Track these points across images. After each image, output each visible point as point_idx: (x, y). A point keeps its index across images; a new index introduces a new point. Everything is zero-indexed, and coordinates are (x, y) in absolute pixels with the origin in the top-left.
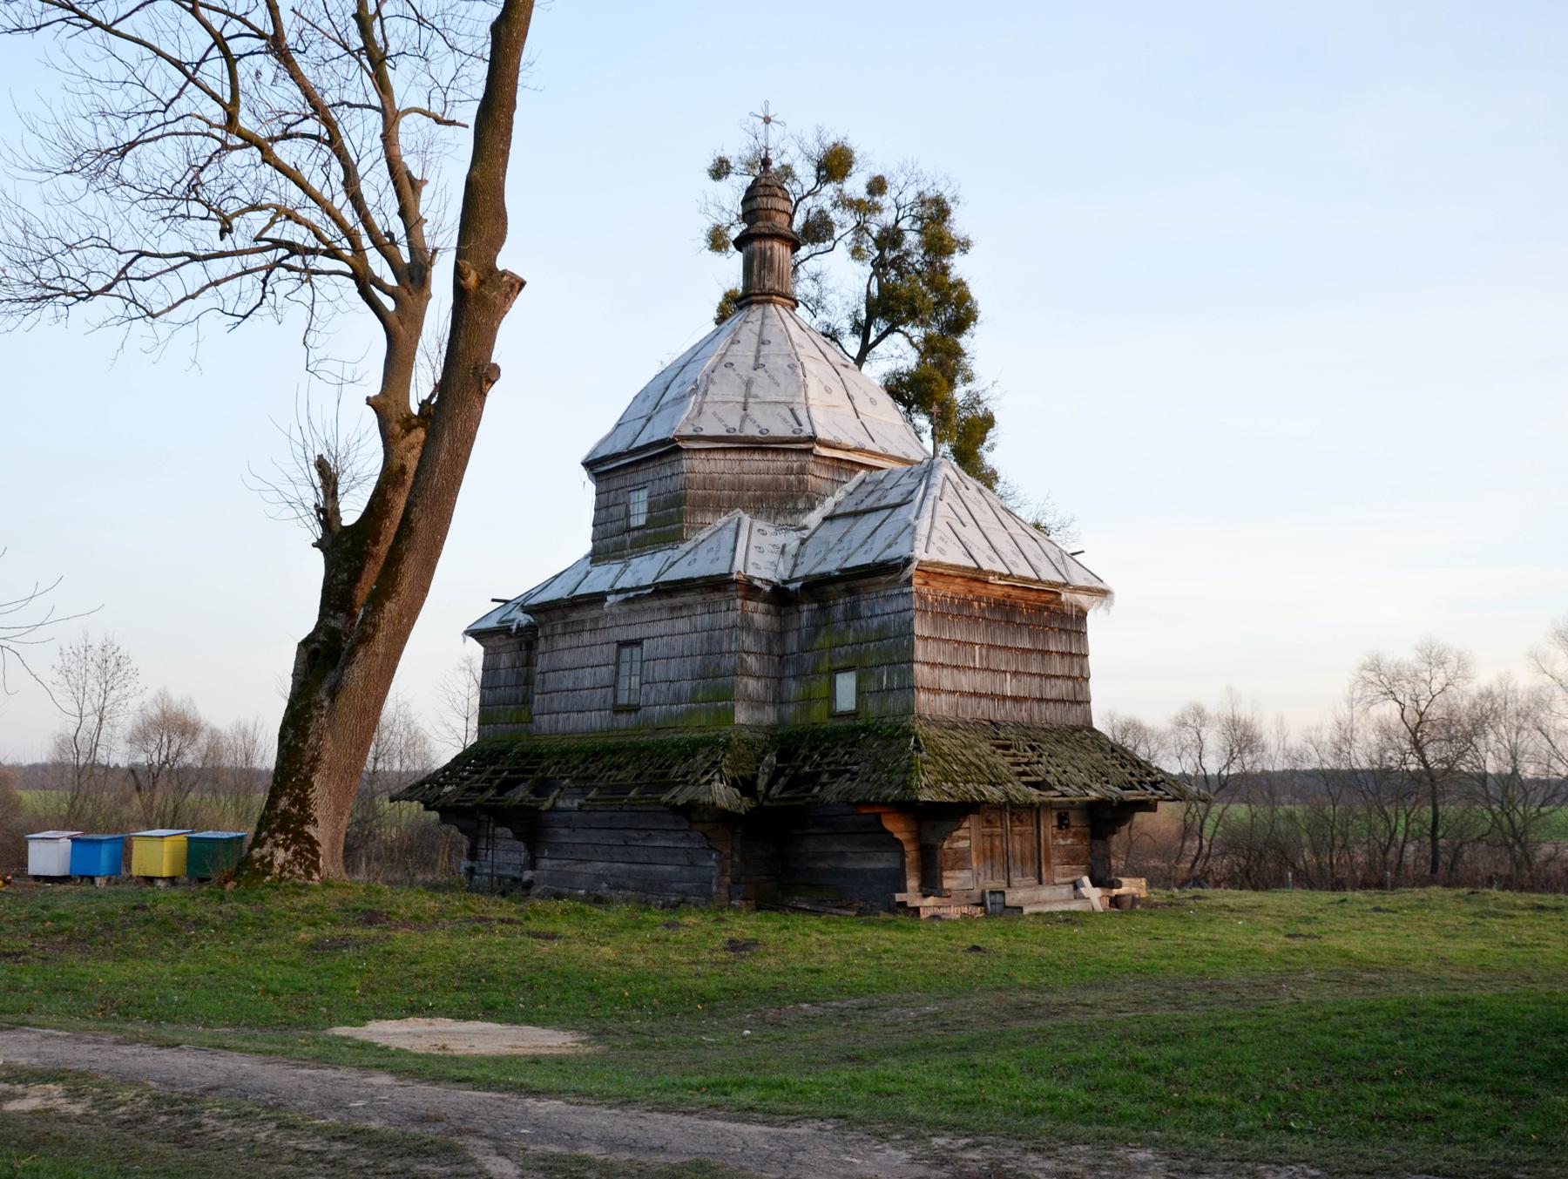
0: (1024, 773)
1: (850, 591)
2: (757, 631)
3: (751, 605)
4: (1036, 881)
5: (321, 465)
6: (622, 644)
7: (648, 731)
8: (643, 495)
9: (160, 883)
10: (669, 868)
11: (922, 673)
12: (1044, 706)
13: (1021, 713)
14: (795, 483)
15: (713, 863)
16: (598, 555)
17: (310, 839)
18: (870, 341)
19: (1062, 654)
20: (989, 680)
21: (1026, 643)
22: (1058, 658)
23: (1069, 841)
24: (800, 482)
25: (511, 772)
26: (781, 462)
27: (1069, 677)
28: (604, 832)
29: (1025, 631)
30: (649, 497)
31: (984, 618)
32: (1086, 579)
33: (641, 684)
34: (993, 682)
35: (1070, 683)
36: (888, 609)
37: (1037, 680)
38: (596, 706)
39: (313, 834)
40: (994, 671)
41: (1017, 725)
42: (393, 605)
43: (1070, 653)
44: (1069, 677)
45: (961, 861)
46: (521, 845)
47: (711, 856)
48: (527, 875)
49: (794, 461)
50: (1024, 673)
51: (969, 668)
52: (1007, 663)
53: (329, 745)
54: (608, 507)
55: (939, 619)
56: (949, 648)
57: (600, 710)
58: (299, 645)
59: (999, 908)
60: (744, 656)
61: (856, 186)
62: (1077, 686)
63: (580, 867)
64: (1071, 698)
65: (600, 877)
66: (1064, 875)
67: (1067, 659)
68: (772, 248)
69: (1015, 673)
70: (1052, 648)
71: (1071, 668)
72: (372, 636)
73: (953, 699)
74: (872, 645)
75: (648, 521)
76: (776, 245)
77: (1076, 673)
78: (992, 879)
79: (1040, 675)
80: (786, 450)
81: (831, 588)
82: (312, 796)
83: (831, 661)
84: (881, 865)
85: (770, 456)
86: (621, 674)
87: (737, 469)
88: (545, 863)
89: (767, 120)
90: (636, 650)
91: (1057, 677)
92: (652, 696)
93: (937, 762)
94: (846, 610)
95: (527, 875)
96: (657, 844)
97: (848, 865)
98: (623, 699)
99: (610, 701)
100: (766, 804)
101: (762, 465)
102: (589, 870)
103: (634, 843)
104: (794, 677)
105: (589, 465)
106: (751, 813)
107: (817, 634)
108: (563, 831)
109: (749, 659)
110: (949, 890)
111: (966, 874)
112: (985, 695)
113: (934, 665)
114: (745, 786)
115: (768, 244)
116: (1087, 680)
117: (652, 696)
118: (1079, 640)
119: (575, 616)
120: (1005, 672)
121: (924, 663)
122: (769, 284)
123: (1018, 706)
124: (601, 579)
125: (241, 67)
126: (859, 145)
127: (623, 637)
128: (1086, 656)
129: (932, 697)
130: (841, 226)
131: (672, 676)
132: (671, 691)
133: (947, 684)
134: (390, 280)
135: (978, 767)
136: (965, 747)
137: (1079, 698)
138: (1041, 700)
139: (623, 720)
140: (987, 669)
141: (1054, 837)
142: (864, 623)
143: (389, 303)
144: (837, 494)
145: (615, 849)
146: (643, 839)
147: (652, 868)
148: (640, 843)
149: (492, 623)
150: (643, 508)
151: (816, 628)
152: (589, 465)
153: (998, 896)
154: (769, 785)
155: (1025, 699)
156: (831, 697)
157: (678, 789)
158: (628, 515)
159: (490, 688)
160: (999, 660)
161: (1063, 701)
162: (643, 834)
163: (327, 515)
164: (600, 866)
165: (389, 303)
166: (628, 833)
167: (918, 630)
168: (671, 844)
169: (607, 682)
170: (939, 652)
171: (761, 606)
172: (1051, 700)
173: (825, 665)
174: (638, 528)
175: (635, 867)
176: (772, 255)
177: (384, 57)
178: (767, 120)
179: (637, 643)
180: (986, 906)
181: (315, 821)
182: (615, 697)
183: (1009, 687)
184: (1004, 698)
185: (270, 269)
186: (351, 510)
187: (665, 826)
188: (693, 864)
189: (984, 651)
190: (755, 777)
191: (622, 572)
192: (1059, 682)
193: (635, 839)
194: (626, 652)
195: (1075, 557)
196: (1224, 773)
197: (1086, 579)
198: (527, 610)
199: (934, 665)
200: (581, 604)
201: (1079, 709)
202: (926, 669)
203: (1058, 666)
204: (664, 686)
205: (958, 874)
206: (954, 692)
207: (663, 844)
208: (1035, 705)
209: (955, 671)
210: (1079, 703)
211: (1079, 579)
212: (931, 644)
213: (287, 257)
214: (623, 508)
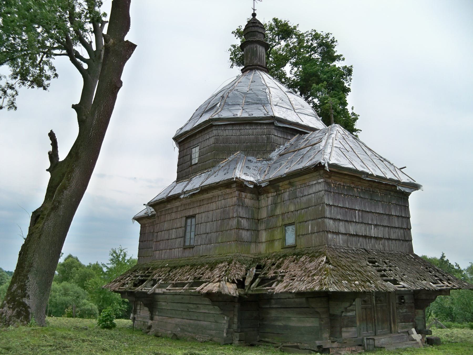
0: (384, 276)
1: (291, 184)
2: (247, 207)
3: (243, 194)
4: (389, 331)
5: (52, 135)
6: (187, 218)
7: (197, 257)
8: (197, 149)
9: (135, 316)
10: (206, 323)
12: (390, 242)
13: (379, 246)
14: (266, 139)
15: (225, 322)
16: (179, 179)
17: (24, 305)
19: (398, 216)
20: (363, 228)
22: (396, 218)
23: (405, 310)
24: (268, 138)
25: (142, 276)
26: (259, 130)
27: (402, 228)
28: (179, 305)
29: (380, 204)
30: (200, 149)
31: (360, 197)
32: (408, 180)
33: (195, 235)
34: (366, 229)
35: (402, 231)
36: (311, 191)
37: (387, 229)
38: (177, 247)
39: (27, 302)
40: (365, 224)
41: (378, 251)
42: (68, 192)
43: (402, 216)
44: (402, 228)
45: (351, 323)
46: (146, 309)
47: (224, 318)
49: (265, 129)
51: (353, 222)
52: (372, 220)
53: (37, 259)
54: (183, 157)
55: (337, 196)
56: (343, 211)
57: (178, 248)
58: (33, 213)
59: (371, 348)
60: (240, 219)
62: (406, 233)
63: (170, 320)
64: (403, 239)
65: (177, 325)
66: (403, 328)
67: (400, 219)
68: (256, 47)
69: (376, 225)
70: (393, 213)
71: (402, 224)
72: (58, 207)
73: (345, 237)
74: (303, 211)
75: (199, 161)
76: (258, 46)
77: (405, 226)
78: (367, 331)
80: (261, 124)
81: (281, 184)
82: (28, 284)
83: (283, 220)
84: (308, 325)
85: (254, 127)
86: (187, 231)
87: (238, 133)
88: (156, 317)
90: (193, 220)
91: (396, 228)
92: (199, 241)
93: (339, 270)
94: (290, 194)
96: (201, 311)
97: (292, 324)
98: (187, 244)
99: (182, 244)
100: (250, 292)
101: (250, 131)
102: (173, 322)
103: (192, 310)
104: (265, 229)
105: (175, 139)
106: (240, 296)
107: (276, 207)
108: (164, 304)
109: (242, 221)
111: (354, 329)
112: (362, 236)
113: (335, 220)
114: (240, 284)
115: (255, 46)
117: (199, 241)
118: (405, 210)
119: (169, 206)
120: (371, 224)
121: (330, 218)
122: (255, 62)
123: (378, 242)
124: (178, 189)
127: (187, 215)
128: (409, 218)
129: (335, 236)
131: (208, 231)
132: (208, 238)
133: (342, 230)
134: (87, 56)
135: (360, 272)
136: (353, 262)
137: (407, 239)
138: (389, 239)
139: (188, 253)
140: (362, 223)
141: (397, 308)
142: (298, 200)
143: (85, 66)
144: (286, 145)
145: (184, 313)
146: (195, 308)
147: (199, 322)
148: (194, 310)
149: (142, 214)
150: (197, 155)
151: (275, 204)
152: (175, 139)
153: (371, 340)
154: (252, 283)
155: (381, 239)
156: (284, 239)
157: (204, 284)
158: (191, 159)
159: (142, 242)
162: (195, 306)
163: (53, 155)
164: (178, 320)
165: (85, 66)
166: (189, 305)
168: (207, 311)
169: (181, 235)
170: (337, 213)
171: (249, 195)
172: (393, 239)
173: (280, 223)
174: (196, 164)
175: (192, 321)
176: (256, 49)
179: (193, 216)
180: (364, 346)
181: (29, 296)
182: (185, 242)
183: (373, 232)
184: (371, 237)
186: (62, 155)
187: (204, 303)
188: (216, 322)
189: (360, 213)
190: (244, 279)
191: (188, 184)
192: (397, 230)
193: (191, 308)
194: (189, 221)
195: (401, 170)
197: (408, 180)
199: (335, 220)
200: (172, 200)
202: (331, 222)
204: (204, 236)
205: (349, 329)
206: (346, 234)
207: (203, 311)
208: (386, 242)
209: (346, 223)
210: (407, 241)
211: (404, 179)
212: (334, 210)
214: (189, 156)
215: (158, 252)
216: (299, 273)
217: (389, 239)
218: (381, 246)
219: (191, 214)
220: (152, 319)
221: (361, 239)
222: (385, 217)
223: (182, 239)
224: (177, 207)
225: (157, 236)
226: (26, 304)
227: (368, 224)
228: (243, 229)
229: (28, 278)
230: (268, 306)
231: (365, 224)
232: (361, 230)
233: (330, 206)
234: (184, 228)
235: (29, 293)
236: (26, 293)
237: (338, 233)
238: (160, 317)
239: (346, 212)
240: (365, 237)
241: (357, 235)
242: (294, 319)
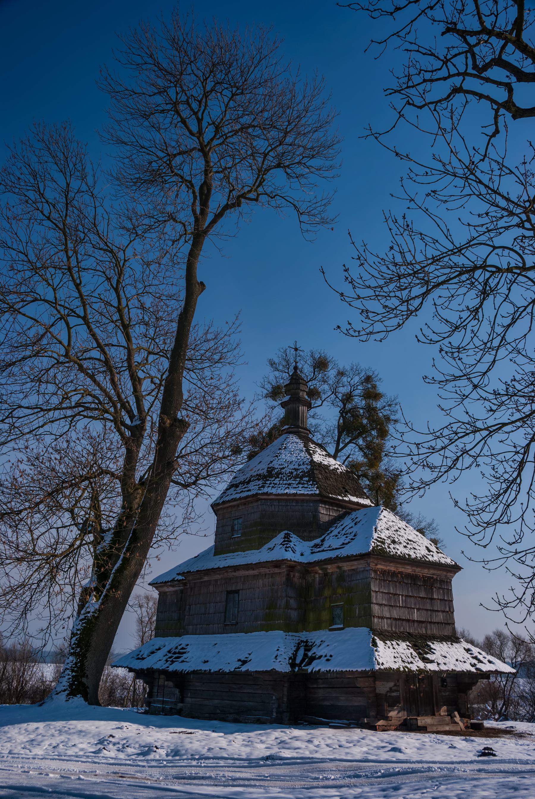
10: (251, 703)
11: (376, 609)
18: (340, 448)
21: (422, 595)
22: (439, 601)
36: (358, 578)
37: (429, 612)
40: (408, 608)
43: (444, 600)
48: (180, 705)
50: (423, 609)
52: (415, 604)
61: (332, 373)
77: (447, 609)
79: (430, 610)
88: (189, 700)
89: (296, 349)
90: (236, 595)
95: (180, 705)
110: (391, 717)
113: (380, 605)
116: (453, 613)
118: (448, 593)
125: (72, 330)
126: (330, 354)
128: (452, 601)
129: (380, 620)
130: (324, 393)
159: (161, 612)
160: (412, 602)
161: (441, 623)
165: (128, 433)
167: (373, 588)
175: (234, 702)
177: (129, 325)
178: (296, 349)
181: (87, 676)
183: (416, 616)
184: (414, 621)
185: (74, 416)
196: (388, 694)
198: (183, 574)
199: (380, 605)
201: (450, 627)
203: (438, 606)
206: (390, 618)
208: (429, 625)
209: (391, 608)
210: (449, 624)
213: (83, 411)
215: (191, 627)
216: (375, 440)
217: (431, 622)
218: (424, 630)
219: (234, 589)
220: (182, 701)
221: (404, 623)
222: (428, 600)
223: (223, 614)
224: (216, 581)
225: (190, 609)
226: (85, 684)
227: (411, 608)
228: (291, 609)
229: (86, 658)
230: (315, 686)
231: (408, 608)
232: (403, 614)
233: (376, 592)
234: (224, 603)
235: (88, 673)
236: (85, 673)
237: (382, 618)
238: (193, 699)
239: (390, 597)
240: (408, 621)
241: (400, 619)
242: (341, 698)
